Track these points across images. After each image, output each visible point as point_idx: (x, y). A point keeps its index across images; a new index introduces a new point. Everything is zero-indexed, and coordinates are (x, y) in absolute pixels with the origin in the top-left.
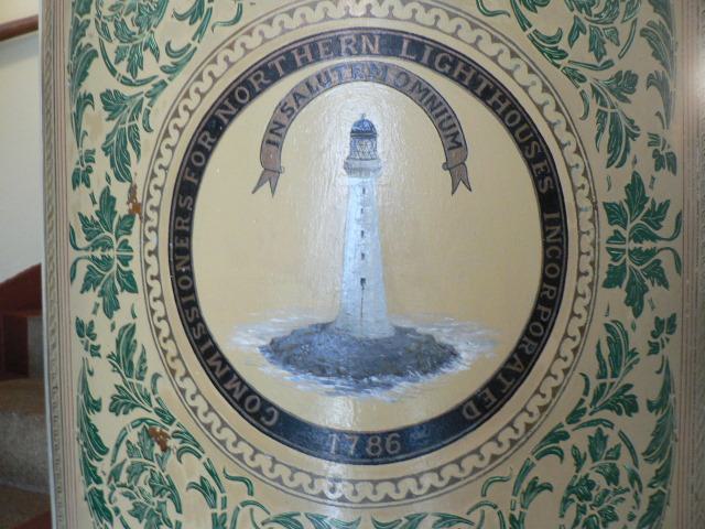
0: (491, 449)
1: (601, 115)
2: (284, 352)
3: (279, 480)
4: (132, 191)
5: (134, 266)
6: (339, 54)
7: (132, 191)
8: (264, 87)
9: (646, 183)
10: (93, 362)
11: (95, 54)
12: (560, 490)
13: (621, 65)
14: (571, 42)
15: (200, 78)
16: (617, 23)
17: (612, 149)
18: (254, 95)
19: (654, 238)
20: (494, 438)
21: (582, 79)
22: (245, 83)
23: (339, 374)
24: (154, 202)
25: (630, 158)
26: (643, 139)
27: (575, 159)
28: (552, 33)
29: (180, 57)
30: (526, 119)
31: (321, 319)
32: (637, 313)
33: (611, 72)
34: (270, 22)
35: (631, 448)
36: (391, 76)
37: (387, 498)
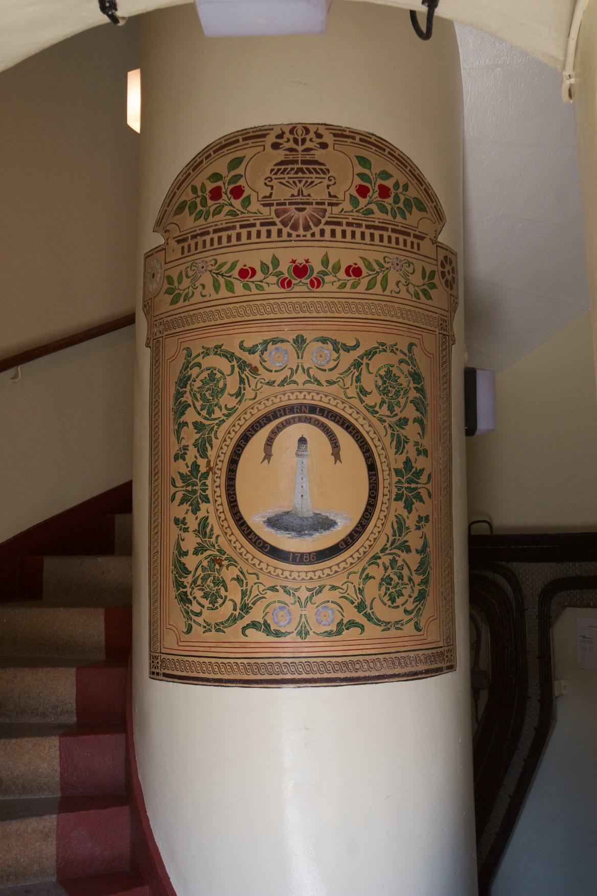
0: (350, 560)
1: (392, 435)
2: (274, 523)
3: (270, 572)
4: (209, 462)
5: (209, 492)
6: (293, 413)
7: (209, 462)
8: (265, 424)
9: (413, 461)
10: (418, 439)
11: (190, 406)
12: (378, 580)
13: (402, 415)
14: (380, 407)
15: (240, 419)
16: (400, 399)
17: (397, 448)
18: (262, 427)
19: (417, 483)
20: (351, 556)
21: (385, 421)
22: (258, 422)
23: (293, 530)
24: (219, 466)
25: (405, 451)
26: (411, 444)
27: (382, 452)
28: (373, 404)
29: (231, 412)
30: (362, 437)
31: (286, 510)
32: (409, 512)
33: (397, 418)
34: (268, 400)
35: (409, 567)
36: (313, 421)
37: (311, 579)
